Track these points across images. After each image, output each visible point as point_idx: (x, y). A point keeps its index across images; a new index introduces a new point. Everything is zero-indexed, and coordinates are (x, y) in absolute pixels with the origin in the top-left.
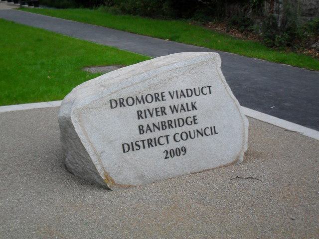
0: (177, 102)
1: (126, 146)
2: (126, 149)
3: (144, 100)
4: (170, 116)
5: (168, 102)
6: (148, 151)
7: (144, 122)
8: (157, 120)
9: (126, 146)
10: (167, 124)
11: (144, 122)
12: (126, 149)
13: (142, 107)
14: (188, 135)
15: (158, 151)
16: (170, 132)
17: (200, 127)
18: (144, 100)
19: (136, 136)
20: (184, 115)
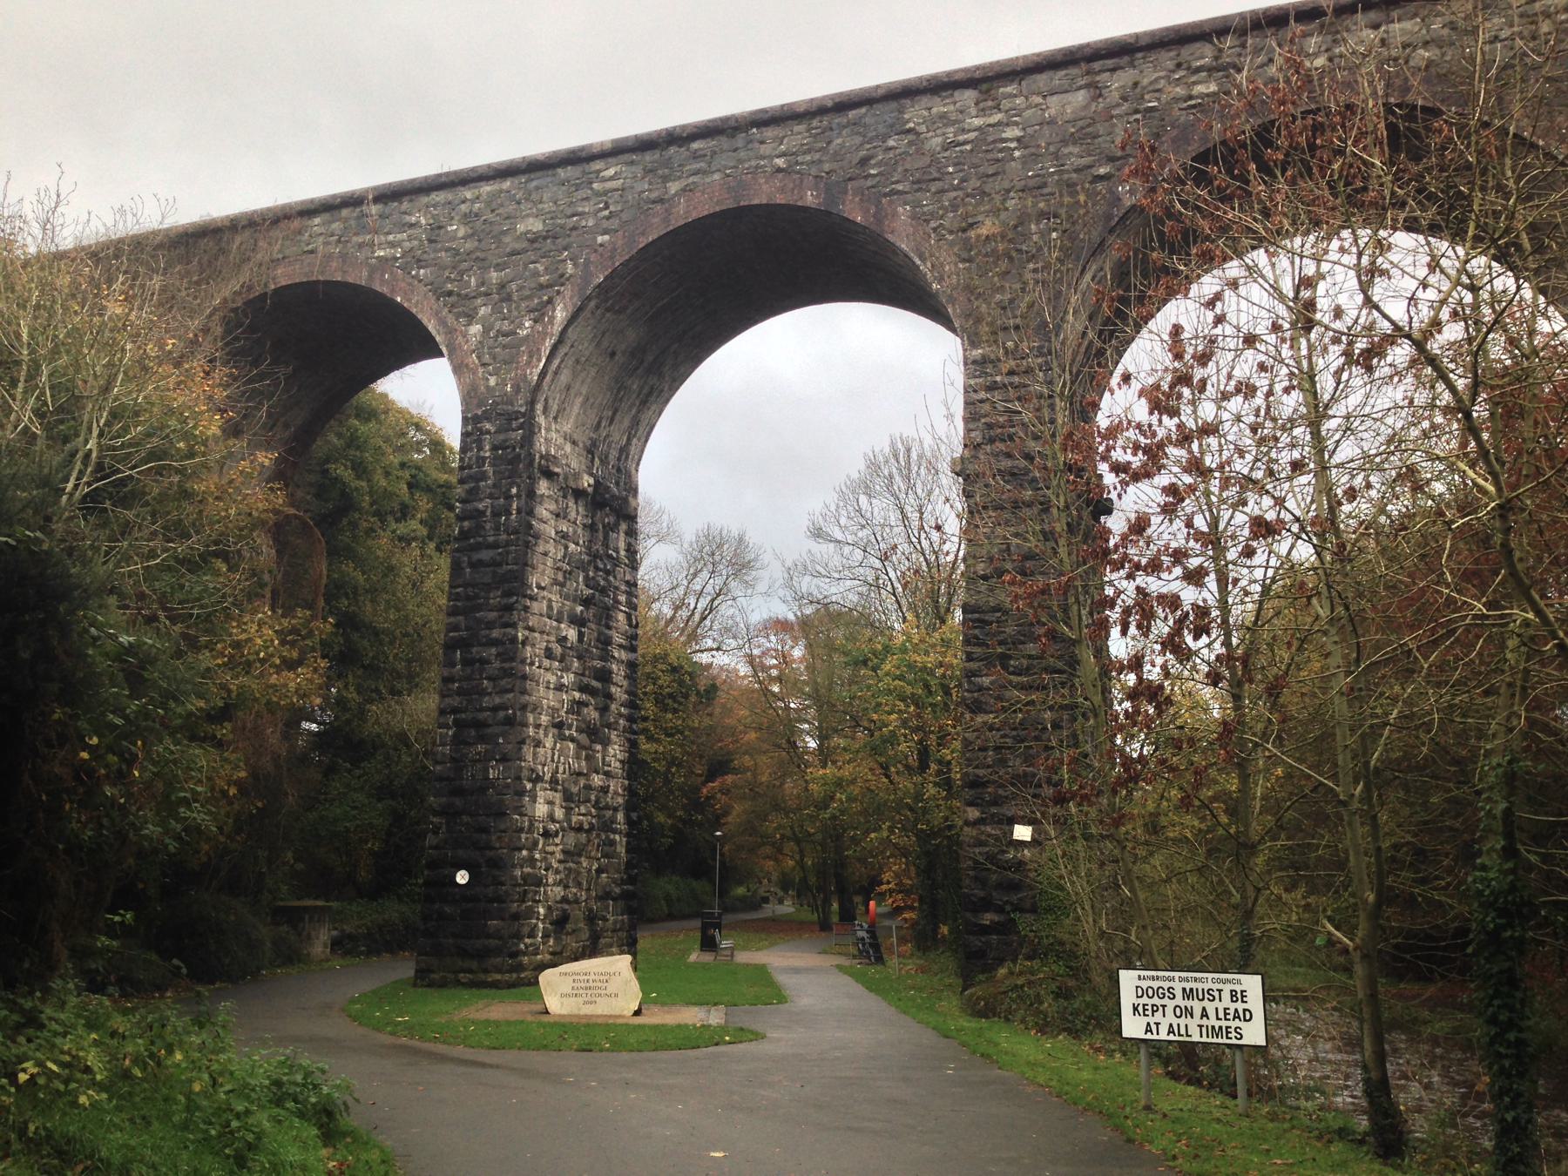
0: (597, 978)
1: (1178, 1010)
2: (1178, 1014)
3: (578, 974)
4: (591, 984)
5: (592, 977)
6: (574, 999)
7: (576, 985)
8: (583, 985)
9: (1178, 1010)
10: (1239, 995)
11: (576, 985)
12: (1178, 1014)
13: (576, 977)
14: (600, 995)
15: (580, 1000)
16: (589, 992)
17: (608, 992)
18: (578, 974)
19: (569, 991)
20: (600, 984)
